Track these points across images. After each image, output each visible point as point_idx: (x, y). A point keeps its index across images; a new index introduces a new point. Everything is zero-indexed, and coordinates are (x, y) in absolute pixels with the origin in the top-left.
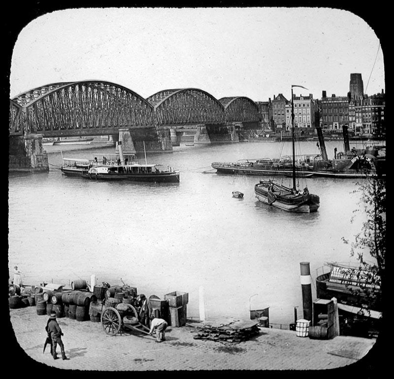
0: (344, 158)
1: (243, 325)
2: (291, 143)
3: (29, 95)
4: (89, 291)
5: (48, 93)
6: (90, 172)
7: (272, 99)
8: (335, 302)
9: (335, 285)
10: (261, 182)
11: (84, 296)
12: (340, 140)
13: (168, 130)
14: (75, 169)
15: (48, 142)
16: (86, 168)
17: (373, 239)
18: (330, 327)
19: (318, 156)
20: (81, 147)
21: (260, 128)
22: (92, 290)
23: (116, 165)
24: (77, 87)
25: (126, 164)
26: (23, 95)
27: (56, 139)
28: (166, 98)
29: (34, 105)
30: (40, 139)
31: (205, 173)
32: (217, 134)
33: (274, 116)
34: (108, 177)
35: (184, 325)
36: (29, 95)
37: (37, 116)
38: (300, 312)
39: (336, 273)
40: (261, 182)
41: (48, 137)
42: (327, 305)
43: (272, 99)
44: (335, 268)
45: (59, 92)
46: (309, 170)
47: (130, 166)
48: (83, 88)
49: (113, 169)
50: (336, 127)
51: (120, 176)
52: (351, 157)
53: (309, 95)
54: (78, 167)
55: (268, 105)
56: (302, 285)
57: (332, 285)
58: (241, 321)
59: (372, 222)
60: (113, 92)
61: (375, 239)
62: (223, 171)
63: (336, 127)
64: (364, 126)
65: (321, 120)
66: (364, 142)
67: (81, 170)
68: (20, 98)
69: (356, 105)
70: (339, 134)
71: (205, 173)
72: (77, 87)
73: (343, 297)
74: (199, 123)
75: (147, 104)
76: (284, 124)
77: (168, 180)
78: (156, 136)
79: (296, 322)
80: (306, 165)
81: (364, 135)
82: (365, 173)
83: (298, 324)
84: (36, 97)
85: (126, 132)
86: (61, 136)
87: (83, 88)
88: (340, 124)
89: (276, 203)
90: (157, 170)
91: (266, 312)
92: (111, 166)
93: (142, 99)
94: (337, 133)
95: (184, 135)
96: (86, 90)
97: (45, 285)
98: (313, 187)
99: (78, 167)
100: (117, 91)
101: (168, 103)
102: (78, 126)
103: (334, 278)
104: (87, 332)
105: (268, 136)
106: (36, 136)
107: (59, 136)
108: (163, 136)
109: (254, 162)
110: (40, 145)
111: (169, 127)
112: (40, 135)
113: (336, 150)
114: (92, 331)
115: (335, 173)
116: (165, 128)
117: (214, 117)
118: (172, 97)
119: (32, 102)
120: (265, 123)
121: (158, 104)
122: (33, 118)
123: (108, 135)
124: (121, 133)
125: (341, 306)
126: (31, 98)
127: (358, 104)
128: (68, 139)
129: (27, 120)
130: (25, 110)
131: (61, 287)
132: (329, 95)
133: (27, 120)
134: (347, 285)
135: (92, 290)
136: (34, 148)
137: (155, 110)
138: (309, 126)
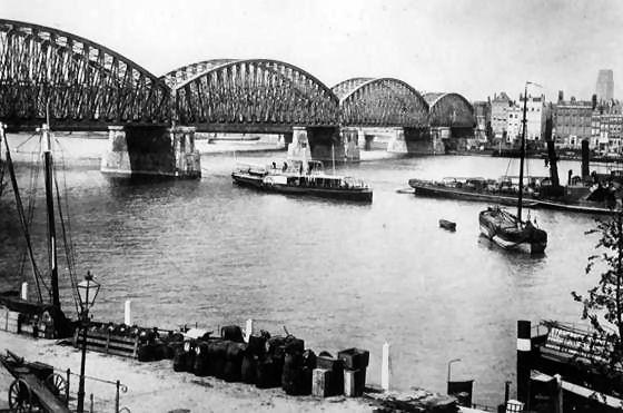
0: (580, 185)
1: (437, 400)
2: (519, 160)
3: (180, 73)
4: (242, 341)
5: (205, 72)
6: (265, 181)
7: (492, 98)
8: (559, 381)
9: (553, 352)
10: (490, 209)
11: (236, 348)
12: (577, 160)
13: (355, 131)
14: (248, 176)
15: (203, 138)
16: (261, 175)
17: (615, 297)
18: (36, 330)
19: (547, 179)
20: (246, 149)
21: (472, 136)
22: (247, 339)
23: (298, 175)
24: (243, 66)
25: (309, 173)
26: (173, 74)
27: (213, 135)
28: (356, 89)
29: (187, 87)
30: (191, 133)
31: (400, 192)
32: (417, 142)
33: (493, 122)
34: (284, 189)
35: (360, 395)
36: (180, 73)
37: (189, 102)
38: (514, 387)
39: (555, 336)
40: (490, 209)
41: (202, 131)
42: (549, 382)
43: (492, 98)
44: (553, 329)
45: (219, 71)
46: (534, 198)
47: (315, 176)
48: (251, 68)
49: (293, 179)
50: (573, 142)
51: (299, 189)
52: (591, 184)
53: (540, 96)
54: (252, 174)
55: (486, 107)
56: (519, 351)
57: (547, 351)
58: (435, 396)
59: (614, 273)
60: (290, 77)
61: (618, 297)
62: (423, 191)
63: (573, 142)
64: (611, 142)
65: (554, 130)
66: (609, 164)
67: (255, 178)
68: (169, 77)
69: (602, 113)
70: (576, 151)
71: (400, 192)
72: (243, 66)
73: (574, 371)
74: (395, 125)
75: (332, 95)
76: (505, 134)
77: (361, 197)
78: (339, 138)
79: (506, 404)
80: (530, 190)
81: (609, 155)
82: (609, 207)
83: (509, 407)
84: (191, 77)
85: (302, 132)
86: (220, 132)
87: (251, 68)
88: (579, 137)
89: (496, 238)
90: (347, 185)
91: (467, 386)
92: (291, 175)
93: (325, 88)
94: (572, 150)
95: (375, 139)
96: (255, 71)
97: (187, 330)
98: (537, 219)
99: (252, 174)
100: (294, 75)
101: (358, 96)
102: (97, 116)
103: (551, 343)
104: (237, 397)
105: (482, 148)
106: (185, 129)
107: (216, 132)
108: (349, 140)
109: (463, 181)
110: (192, 142)
111: (357, 128)
112: (193, 128)
113: (570, 172)
114: (244, 397)
115: (567, 204)
116: (351, 129)
117: (417, 117)
118: (363, 88)
119: (185, 82)
120: (479, 130)
121: (346, 97)
122: (184, 104)
123: (279, 133)
124: (295, 133)
125: (567, 386)
126: (184, 77)
127: (605, 112)
128: (229, 136)
129: (176, 106)
130: (174, 93)
131: (207, 335)
132: (567, 98)
133: (176, 106)
134: (576, 355)
135: (247, 339)
136: (183, 145)
137: (341, 103)
138: (537, 138)
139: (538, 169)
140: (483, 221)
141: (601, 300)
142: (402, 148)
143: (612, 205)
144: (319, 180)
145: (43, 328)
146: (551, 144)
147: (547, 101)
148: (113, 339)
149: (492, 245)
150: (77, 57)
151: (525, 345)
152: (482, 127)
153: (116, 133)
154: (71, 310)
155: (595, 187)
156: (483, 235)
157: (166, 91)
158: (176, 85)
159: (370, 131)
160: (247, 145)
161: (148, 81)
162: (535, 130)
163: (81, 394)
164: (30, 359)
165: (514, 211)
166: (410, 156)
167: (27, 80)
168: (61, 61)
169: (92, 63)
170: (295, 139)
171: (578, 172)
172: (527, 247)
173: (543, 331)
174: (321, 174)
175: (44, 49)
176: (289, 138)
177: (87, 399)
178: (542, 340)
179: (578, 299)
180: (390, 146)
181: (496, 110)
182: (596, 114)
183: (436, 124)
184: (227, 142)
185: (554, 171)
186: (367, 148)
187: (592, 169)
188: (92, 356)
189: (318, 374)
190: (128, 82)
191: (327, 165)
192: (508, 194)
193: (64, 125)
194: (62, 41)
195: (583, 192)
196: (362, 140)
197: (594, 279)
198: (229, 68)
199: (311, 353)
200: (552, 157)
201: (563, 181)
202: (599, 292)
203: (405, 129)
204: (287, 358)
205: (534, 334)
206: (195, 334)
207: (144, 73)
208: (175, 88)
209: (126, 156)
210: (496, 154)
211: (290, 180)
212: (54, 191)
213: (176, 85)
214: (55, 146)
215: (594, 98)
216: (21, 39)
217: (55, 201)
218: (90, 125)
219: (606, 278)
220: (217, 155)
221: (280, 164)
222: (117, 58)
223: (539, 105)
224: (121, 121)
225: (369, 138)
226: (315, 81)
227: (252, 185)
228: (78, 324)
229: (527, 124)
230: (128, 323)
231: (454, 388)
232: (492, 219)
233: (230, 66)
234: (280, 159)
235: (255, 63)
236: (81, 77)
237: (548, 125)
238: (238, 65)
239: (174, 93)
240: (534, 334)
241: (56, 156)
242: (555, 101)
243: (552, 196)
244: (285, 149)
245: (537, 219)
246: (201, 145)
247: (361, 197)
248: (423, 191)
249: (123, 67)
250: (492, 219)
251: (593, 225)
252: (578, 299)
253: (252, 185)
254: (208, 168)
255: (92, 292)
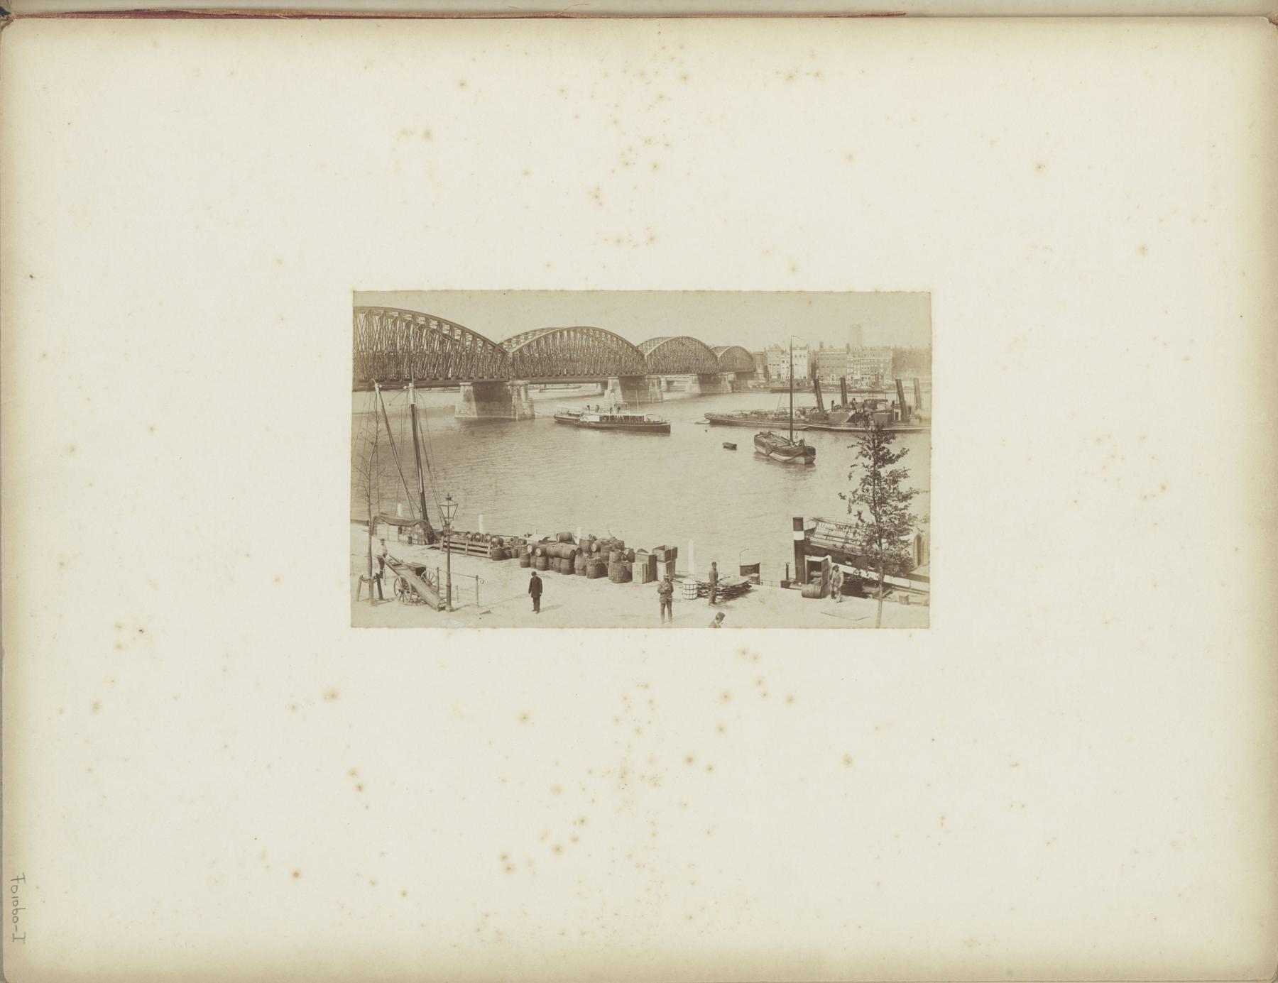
21: (752, 378)
23: (608, 414)
26: (509, 340)
29: (520, 350)
32: (709, 381)
45: (546, 337)
51: (609, 425)
55: (763, 355)
62: (715, 422)
77: (662, 429)
84: (523, 343)
89: (773, 455)
91: (756, 568)
93: (632, 347)
98: (809, 439)
126: (518, 343)
128: (556, 386)
132: (826, 346)
139: (806, 400)
140: (757, 442)
141: (861, 498)
142: (696, 389)
143: (867, 424)
144: (626, 417)
145: (416, 537)
146: (816, 382)
147: (811, 349)
148: (474, 544)
149: (770, 460)
150: (433, 331)
151: (800, 536)
152: (760, 370)
153: (466, 388)
154: (437, 526)
155: (852, 413)
156: (758, 453)
157: (504, 353)
158: (512, 350)
159: (670, 377)
160: (576, 392)
161: (490, 347)
162: (802, 371)
163: (449, 587)
164: (407, 561)
165: (786, 434)
166: (702, 395)
167: (395, 351)
168: (421, 336)
169: (445, 336)
170: (610, 387)
171: (838, 402)
172: (802, 460)
173: (812, 525)
174: (628, 413)
175: (408, 327)
176: (605, 385)
177: (453, 589)
178: (812, 531)
179: (843, 498)
180: (687, 389)
181: (770, 355)
182: (850, 357)
183: (723, 370)
184: (554, 391)
185: (820, 401)
186: (668, 391)
187: (849, 400)
188: (455, 557)
189: (637, 568)
190: (473, 349)
191: (632, 405)
192: (787, 421)
193: (424, 383)
194: (434, 325)
195: (842, 416)
196: (664, 384)
197: (856, 483)
198: (554, 334)
199: (631, 551)
200: (817, 389)
201: (827, 406)
202: (860, 492)
203: (621, 378)
204: (612, 555)
205: (806, 528)
206: (536, 538)
207: (485, 341)
208: (511, 351)
209: (474, 404)
210: (774, 391)
211: (602, 418)
212: (419, 435)
213: (512, 350)
214: (419, 400)
215: (848, 346)
216: (390, 321)
217: (421, 443)
218: (449, 384)
219: (864, 481)
220: (547, 400)
221: (593, 406)
222: (464, 331)
223: (805, 352)
224: (470, 378)
225: (669, 383)
226: (624, 341)
227: (572, 422)
228: (442, 533)
229: (795, 367)
230: (482, 532)
231: (745, 570)
232: (765, 440)
233: (554, 333)
234: (593, 403)
235: (575, 329)
236: (436, 346)
237: (814, 368)
238: (561, 332)
239: (510, 355)
240: (806, 528)
241: (420, 405)
242: (817, 348)
243: (821, 421)
244: (602, 394)
245: (809, 439)
246: (534, 394)
247: (662, 429)
248: (715, 422)
249: (470, 337)
250: (765, 440)
251: (854, 441)
252: (843, 498)
253: (572, 422)
254: (540, 410)
255: (452, 509)
